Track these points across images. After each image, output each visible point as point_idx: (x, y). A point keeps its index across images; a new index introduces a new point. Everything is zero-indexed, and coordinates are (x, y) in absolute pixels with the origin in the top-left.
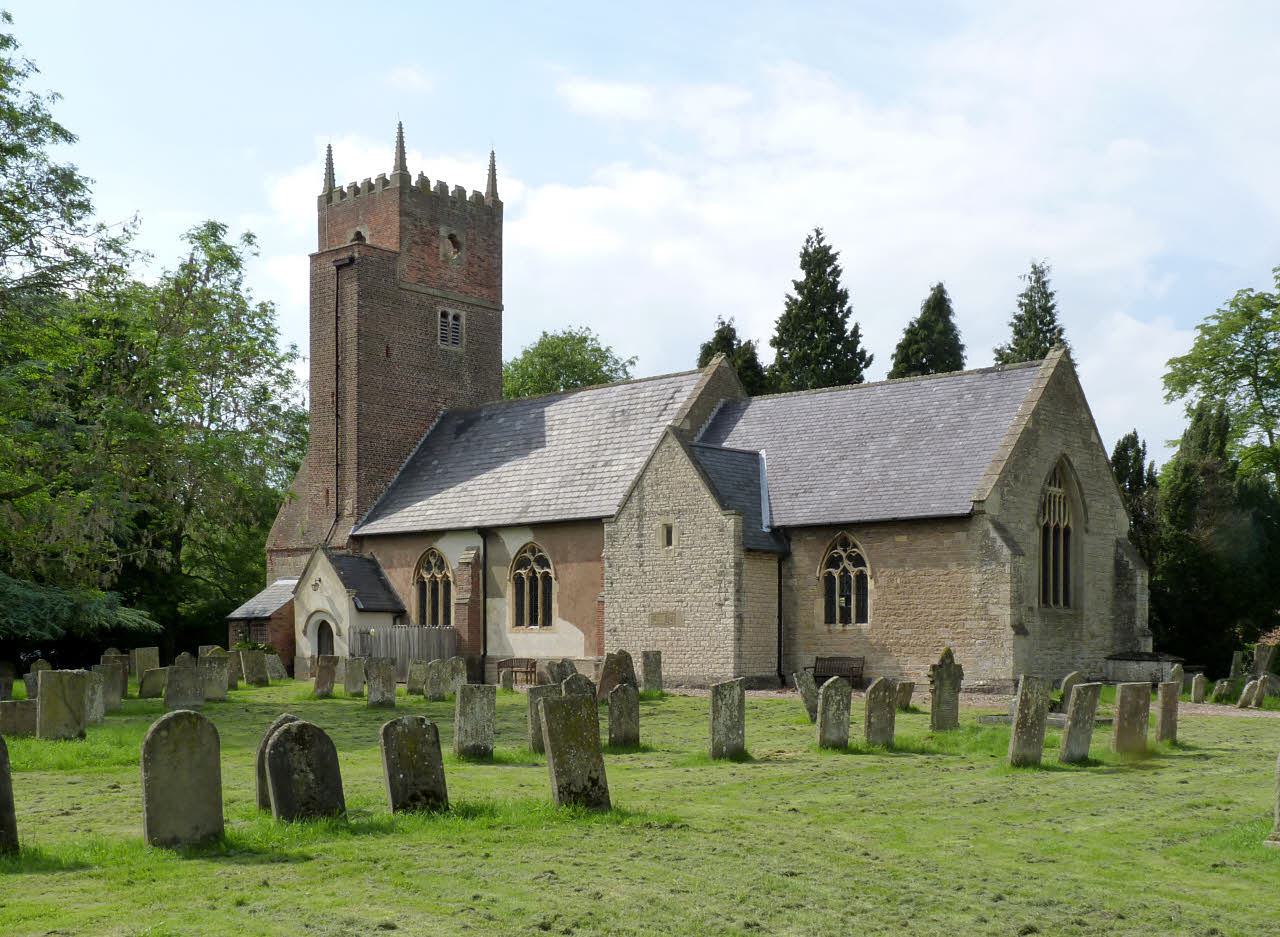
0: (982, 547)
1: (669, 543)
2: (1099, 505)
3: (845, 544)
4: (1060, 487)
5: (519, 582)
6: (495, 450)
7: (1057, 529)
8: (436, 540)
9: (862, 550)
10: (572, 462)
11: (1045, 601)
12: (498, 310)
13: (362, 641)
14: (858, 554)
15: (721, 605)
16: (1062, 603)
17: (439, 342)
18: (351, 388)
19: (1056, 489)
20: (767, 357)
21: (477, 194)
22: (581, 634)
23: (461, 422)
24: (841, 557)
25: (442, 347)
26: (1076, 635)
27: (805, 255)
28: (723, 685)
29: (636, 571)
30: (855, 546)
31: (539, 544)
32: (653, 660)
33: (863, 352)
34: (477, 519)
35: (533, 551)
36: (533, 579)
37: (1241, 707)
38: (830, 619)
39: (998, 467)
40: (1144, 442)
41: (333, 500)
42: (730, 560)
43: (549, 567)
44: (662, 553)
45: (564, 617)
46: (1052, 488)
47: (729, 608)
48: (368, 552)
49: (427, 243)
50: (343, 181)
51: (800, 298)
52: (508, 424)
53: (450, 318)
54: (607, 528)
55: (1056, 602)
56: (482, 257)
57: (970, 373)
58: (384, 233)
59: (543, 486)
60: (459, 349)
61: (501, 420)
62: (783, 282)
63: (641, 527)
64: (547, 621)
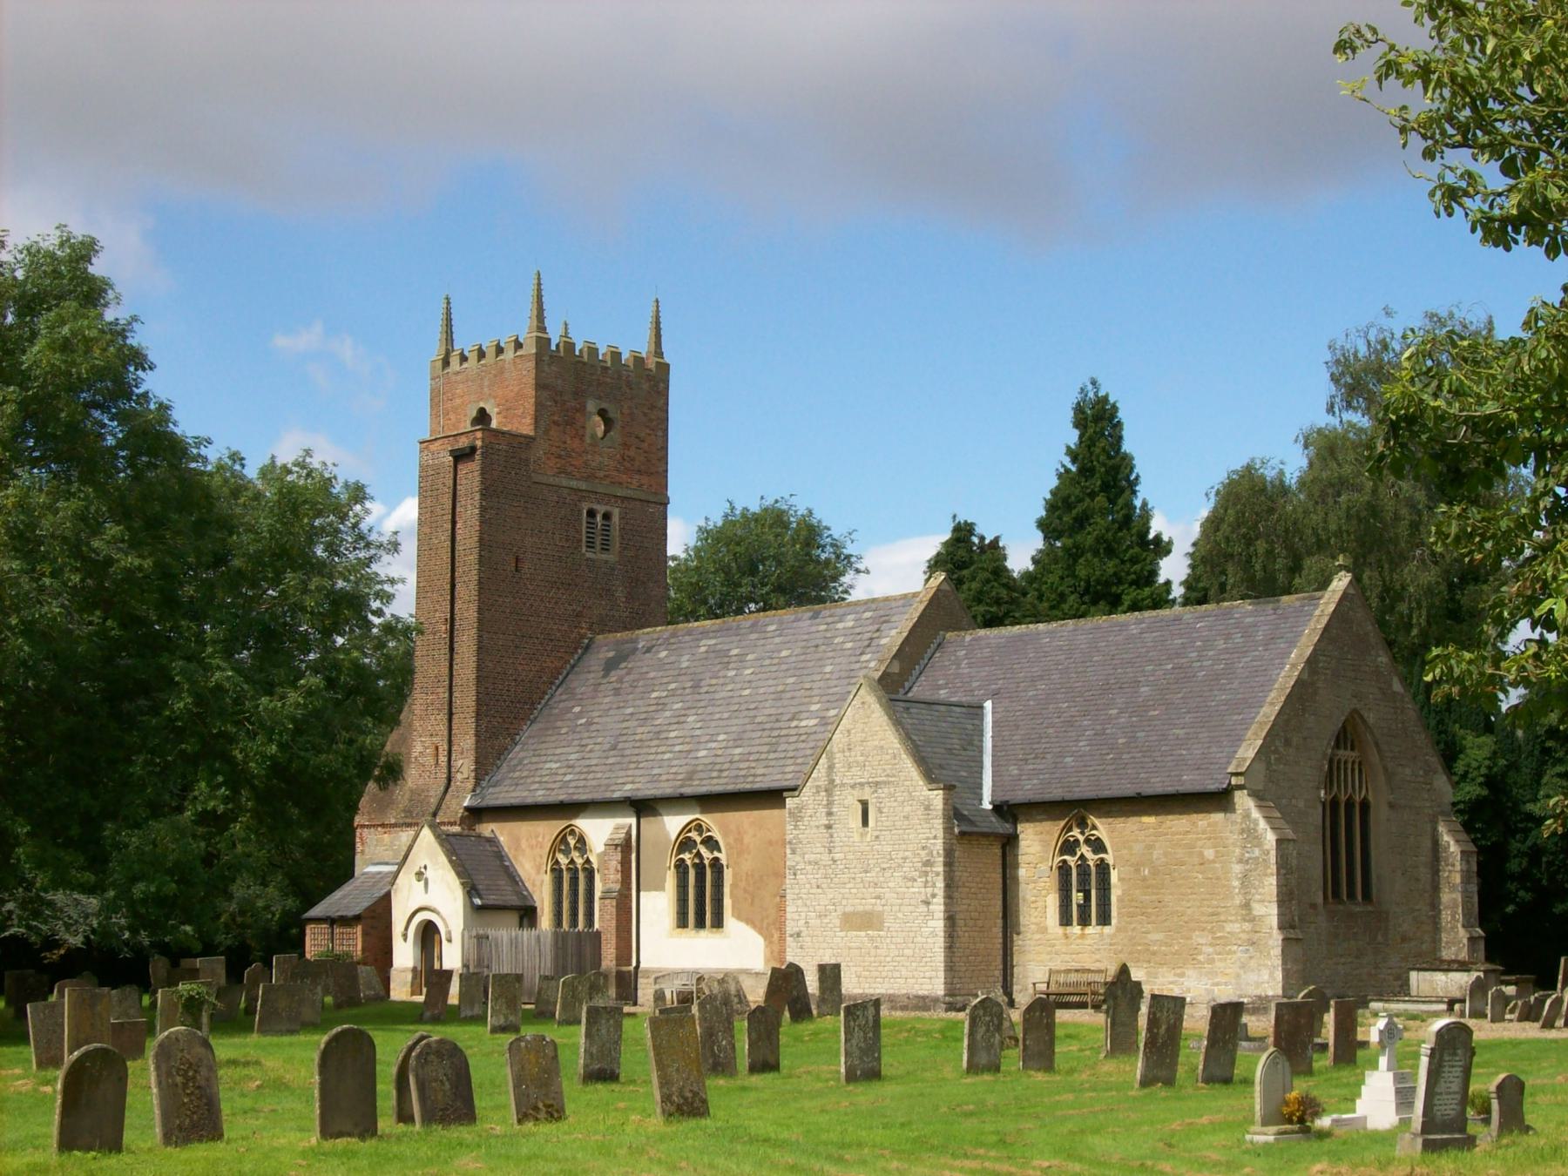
0: (1243, 831)
1: (865, 822)
2: (1408, 771)
5: (681, 867)
6: (654, 695)
7: (1349, 804)
8: (576, 816)
10: (752, 713)
13: (479, 945)
15: (927, 903)
16: (1360, 898)
18: (468, 613)
20: (1021, 557)
21: (639, 360)
22: (760, 940)
24: (1077, 841)
25: (589, 555)
26: (1380, 938)
27: (1079, 409)
28: (855, 1006)
29: (826, 858)
30: (1094, 827)
32: (830, 974)
33: (1158, 538)
34: (628, 787)
35: (699, 828)
36: (574, 872)
37: (1543, 1027)
38: (1065, 920)
41: (443, 759)
42: (938, 846)
44: (856, 838)
45: (738, 915)
46: (1341, 752)
47: (938, 906)
48: (487, 829)
49: (570, 422)
51: (1074, 469)
52: (672, 659)
53: (599, 518)
55: (1351, 895)
56: (642, 435)
58: (515, 413)
59: (713, 745)
60: (611, 557)
61: (663, 654)
62: (1050, 450)
63: (830, 804)
64: (718, 923)
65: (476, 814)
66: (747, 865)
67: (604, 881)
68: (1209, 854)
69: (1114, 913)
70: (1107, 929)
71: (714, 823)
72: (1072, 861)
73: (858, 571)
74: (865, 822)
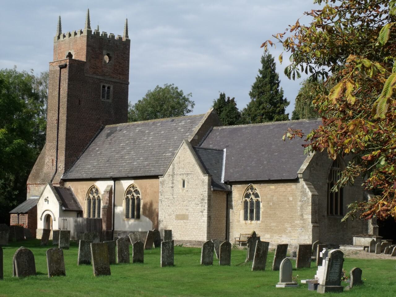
0: (301, 192)
1: (184, 186)
3: (252, 189)
4: (338, 167)
5: (127, 199)
6: (121, 145)
9: (258, 191)
11: (331, 213)
12: (126, 84)
14: (257, 193)
17: (101, 98)
19: (337, 168)
23: (109, 131)
25: (103, 100)
27: (263, 59)
31: (136, 185)
34: (112, 173)
36: (252, 203)
38: (246, 218)
39: (309, 160)
40: (41, 220)
41: (55, 163)
42: (206, 194)
43: (139, 194)
46: (335, 168)
47: (205, 213)
52: (128, 133)
53: (106, 88)
55: (336, 213)
57: (177, 147)
59: (139, 161)
60: (110, 101)
61: (125, 132)
63: (173, 180)
68: (291, 199)
69: (261, 217)
70: (258, 222)
72: (248, 200)
74: (184, 186)
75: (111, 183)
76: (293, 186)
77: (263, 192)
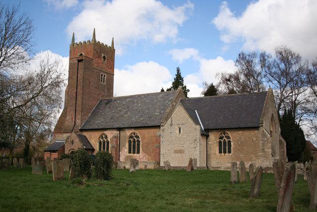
1: (180, 131)
5: (130, 142)
35: (134, 134)
36: (134, 141)
38: (220, 152)
41: (74, 120)
50: (77, 41)
54: (161, 128)
57: (174, 107)
65: (81, 130)
66: (145, 141)
67: (112, 144)
68: (254, 139)
69: (232, 150)
70: (230, 154)
71: (137, 132)
72: (222, 141)
73: (250, 73)
74: (180, 131)
75: (116, 132)
76: (253, 133)
77: (234, 137)
